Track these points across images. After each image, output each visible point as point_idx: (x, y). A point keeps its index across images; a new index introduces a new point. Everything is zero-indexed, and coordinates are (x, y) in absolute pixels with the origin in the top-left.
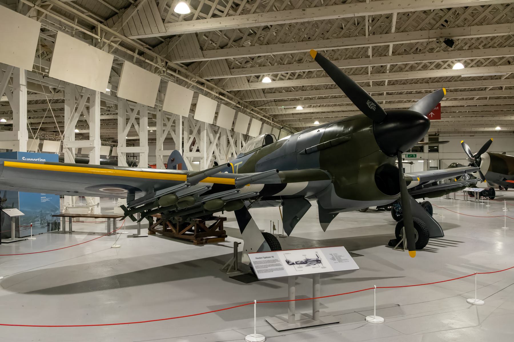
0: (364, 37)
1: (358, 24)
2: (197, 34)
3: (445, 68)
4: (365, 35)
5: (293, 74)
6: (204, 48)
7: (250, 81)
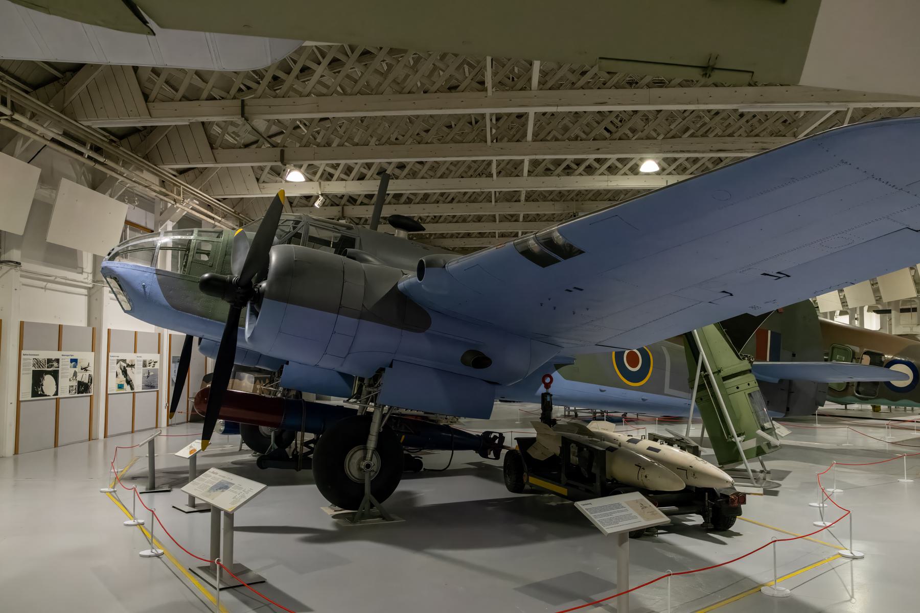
0: (482, 144)
1: (476, 123)
2: (136, 69)
3: (625, 174)
4: (486, 142)
5: (349, 170)
6: (152, 97)
7: (261, 180)
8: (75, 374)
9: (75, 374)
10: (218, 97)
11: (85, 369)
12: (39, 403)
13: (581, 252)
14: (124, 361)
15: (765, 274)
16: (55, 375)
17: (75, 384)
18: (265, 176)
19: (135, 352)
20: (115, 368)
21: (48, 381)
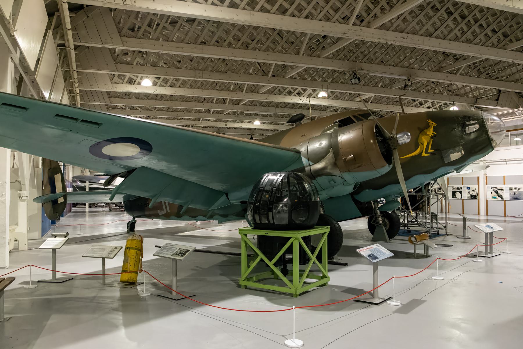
8: (469, 192)
9: (469, 192)
10: (243, 288)
11: (474, 191)
12: (455, 200)
13: (102, 124)
14: (496, 188)
15: (57, 115)
16: (461, 192)
17: (469, 195)
18: (116, 78)
19: (504, 184)
20: (490, 190)
21: (458, 195)
